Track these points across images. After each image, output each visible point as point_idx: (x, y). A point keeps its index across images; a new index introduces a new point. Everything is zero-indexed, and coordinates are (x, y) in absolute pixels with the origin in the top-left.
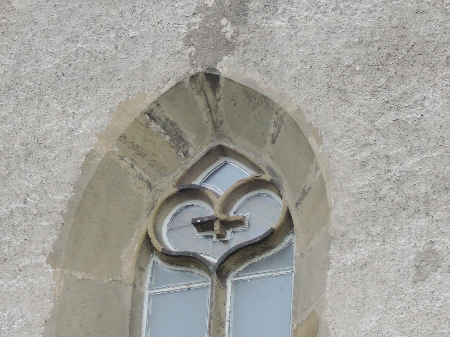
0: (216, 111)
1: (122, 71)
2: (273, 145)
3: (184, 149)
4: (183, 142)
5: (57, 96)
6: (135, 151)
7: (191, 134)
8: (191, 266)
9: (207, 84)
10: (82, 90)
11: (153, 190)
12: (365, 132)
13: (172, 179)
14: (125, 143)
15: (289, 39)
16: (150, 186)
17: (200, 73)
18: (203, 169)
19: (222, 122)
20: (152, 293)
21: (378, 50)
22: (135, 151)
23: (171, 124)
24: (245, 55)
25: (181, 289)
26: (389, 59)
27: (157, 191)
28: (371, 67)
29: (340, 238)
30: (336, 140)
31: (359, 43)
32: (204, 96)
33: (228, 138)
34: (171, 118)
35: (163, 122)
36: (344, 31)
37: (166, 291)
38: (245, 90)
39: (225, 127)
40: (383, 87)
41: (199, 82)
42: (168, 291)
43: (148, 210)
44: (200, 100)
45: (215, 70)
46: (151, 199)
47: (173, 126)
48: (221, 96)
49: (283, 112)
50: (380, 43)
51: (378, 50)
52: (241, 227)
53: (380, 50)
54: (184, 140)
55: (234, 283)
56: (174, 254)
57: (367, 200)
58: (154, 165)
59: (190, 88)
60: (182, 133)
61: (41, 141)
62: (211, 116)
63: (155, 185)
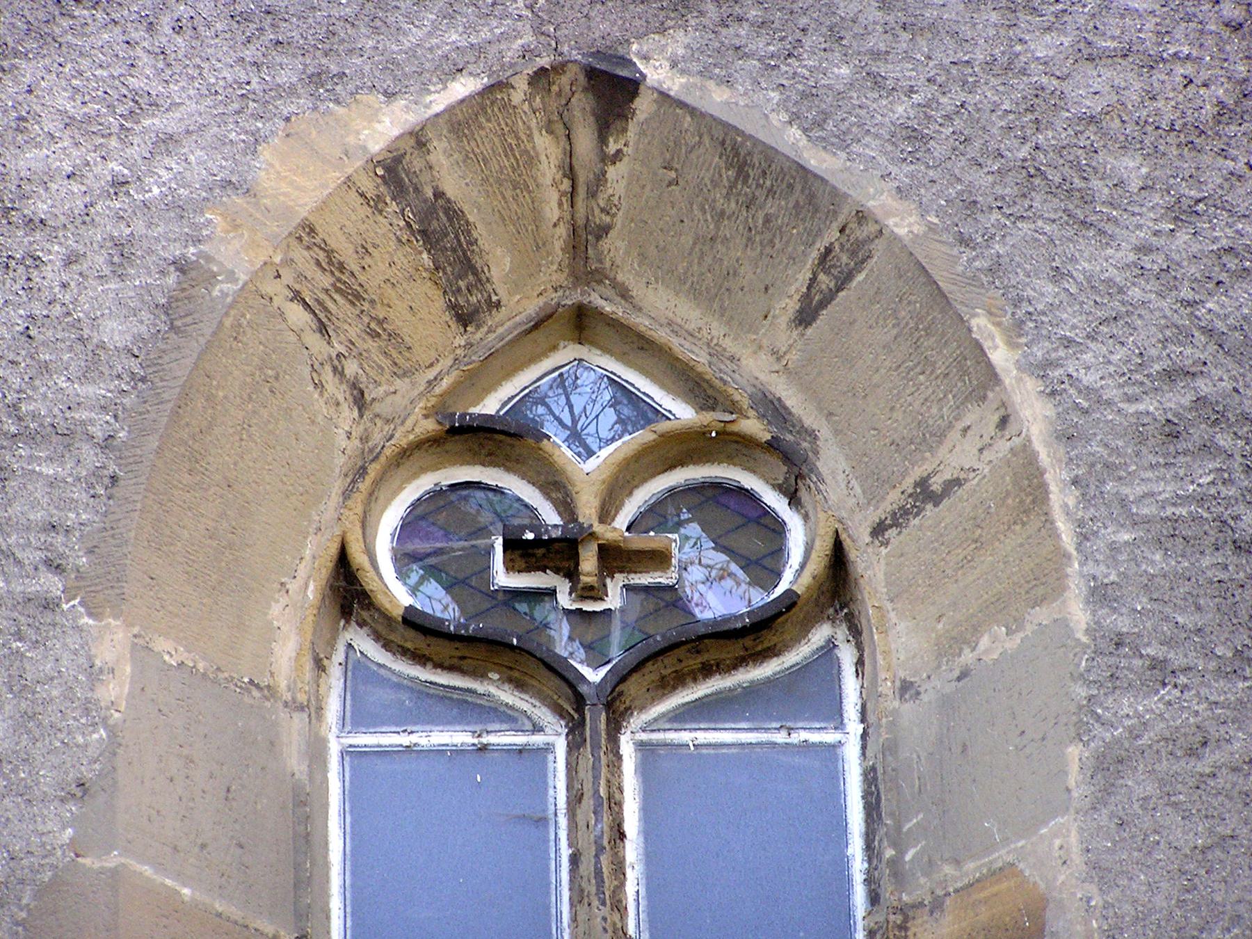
0: (592, 194)
1: (287, 17)
2: (801, 328)
3: (470, 298)
4: (471, 277)
5: (61, 65)
6: (332, 280)
7: (499, 251)
8: (490, 675)
9: (582, 106)
10: (145, 58)
11: (368, 415)
12: (1168, 333)
13: (422, 388)
14: (308, 248)
15: (877, 5)
16: (360, 400)
17: (570, 65)
18: (509, 374)
19: (605, 230)
20: (351, 746)
21: (1185, 86)
22: (332, 280)
23: (447, 211)
24: (724, 31)
25: (691, 730)
26: (1223, 118)
27: (377, 420)
28: (1164, 134)
29: (1111, 649)
30: (1069, 342)
31: (1119, 53)
32: (564, 139)
33: (615, 285)
34: (451, 191)
35: (425, 201)
36: (1066, 10)
37: (401, 746)
38: (728, 142)
39: (614, 247)
40: (1210, 202)
41: (559, 94)
42: (407, 747)
43: (346, 475)
44: (547, 149)
45: (627, 62)
46: (357, 442)
47: (450, 219)
48: (625, 149)
49: (871, 228)
50: (1189, 65)
51: (1185, 86)
52: (658, 574)
53: (1191, 88)
54: (476, 269)
55: (641, 746)
56: (452, 628)
57: (1193, 546)
58: (379, 335)
59: (526, 106)
60: (475, 247)
61: (12, 201)
62: (572, 207)
63: (374, 400)
